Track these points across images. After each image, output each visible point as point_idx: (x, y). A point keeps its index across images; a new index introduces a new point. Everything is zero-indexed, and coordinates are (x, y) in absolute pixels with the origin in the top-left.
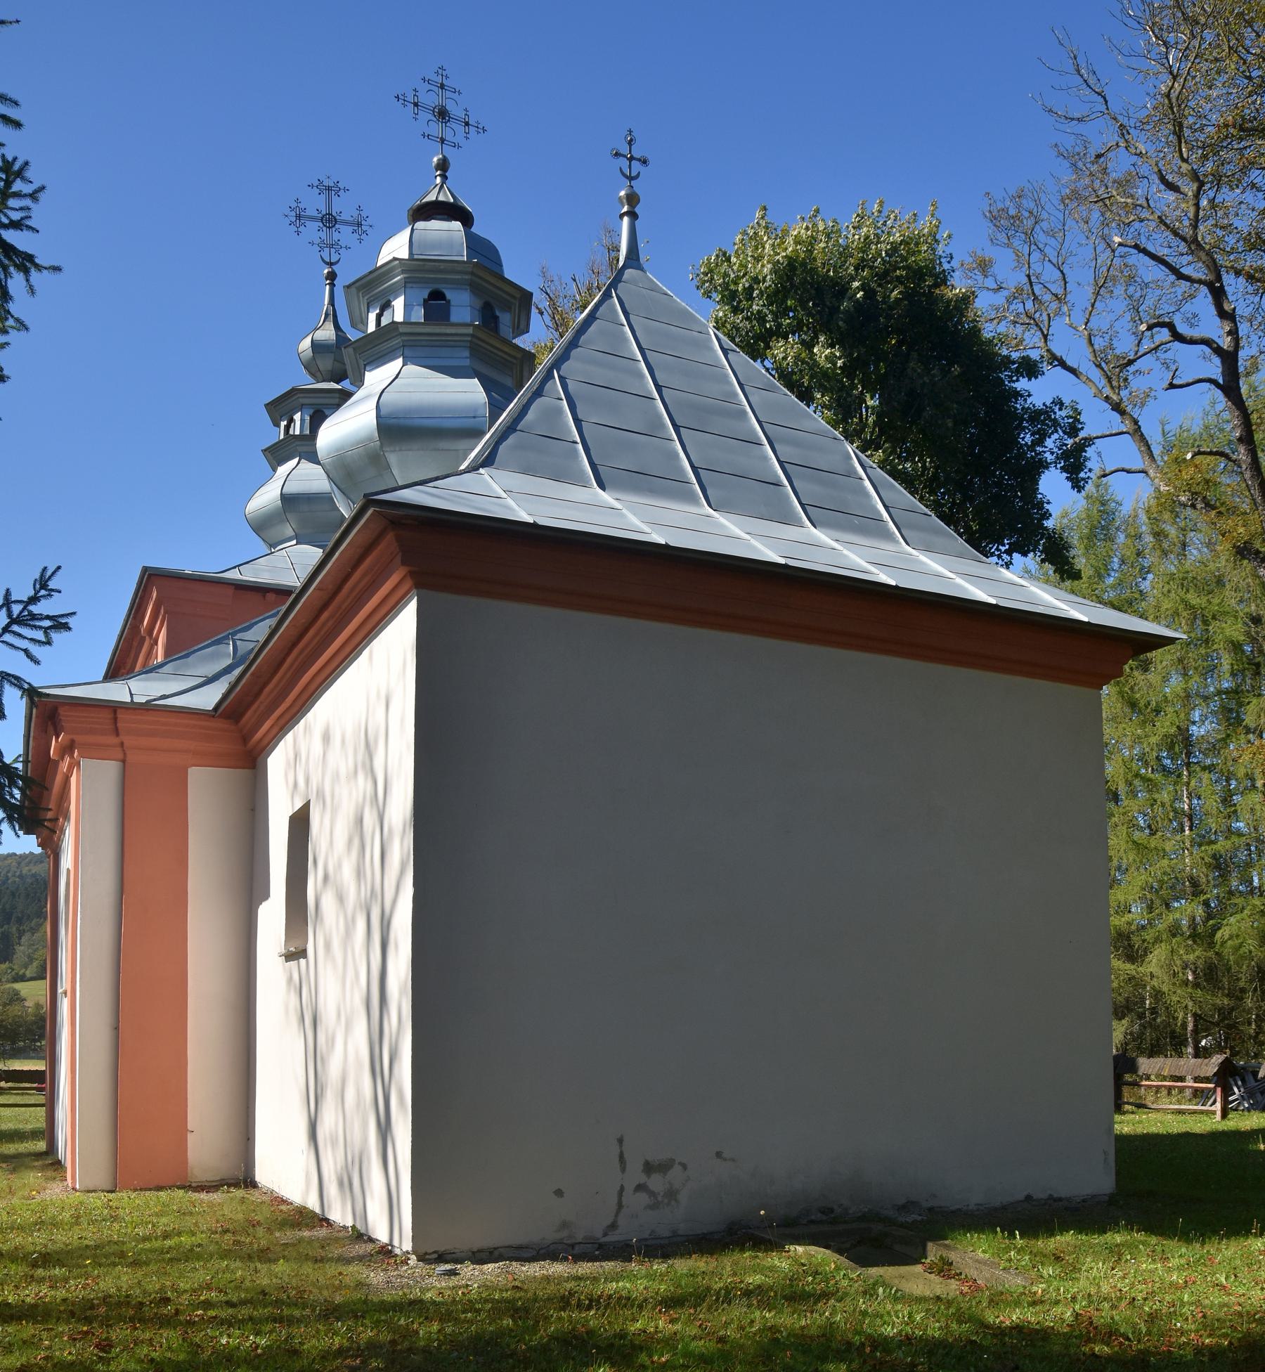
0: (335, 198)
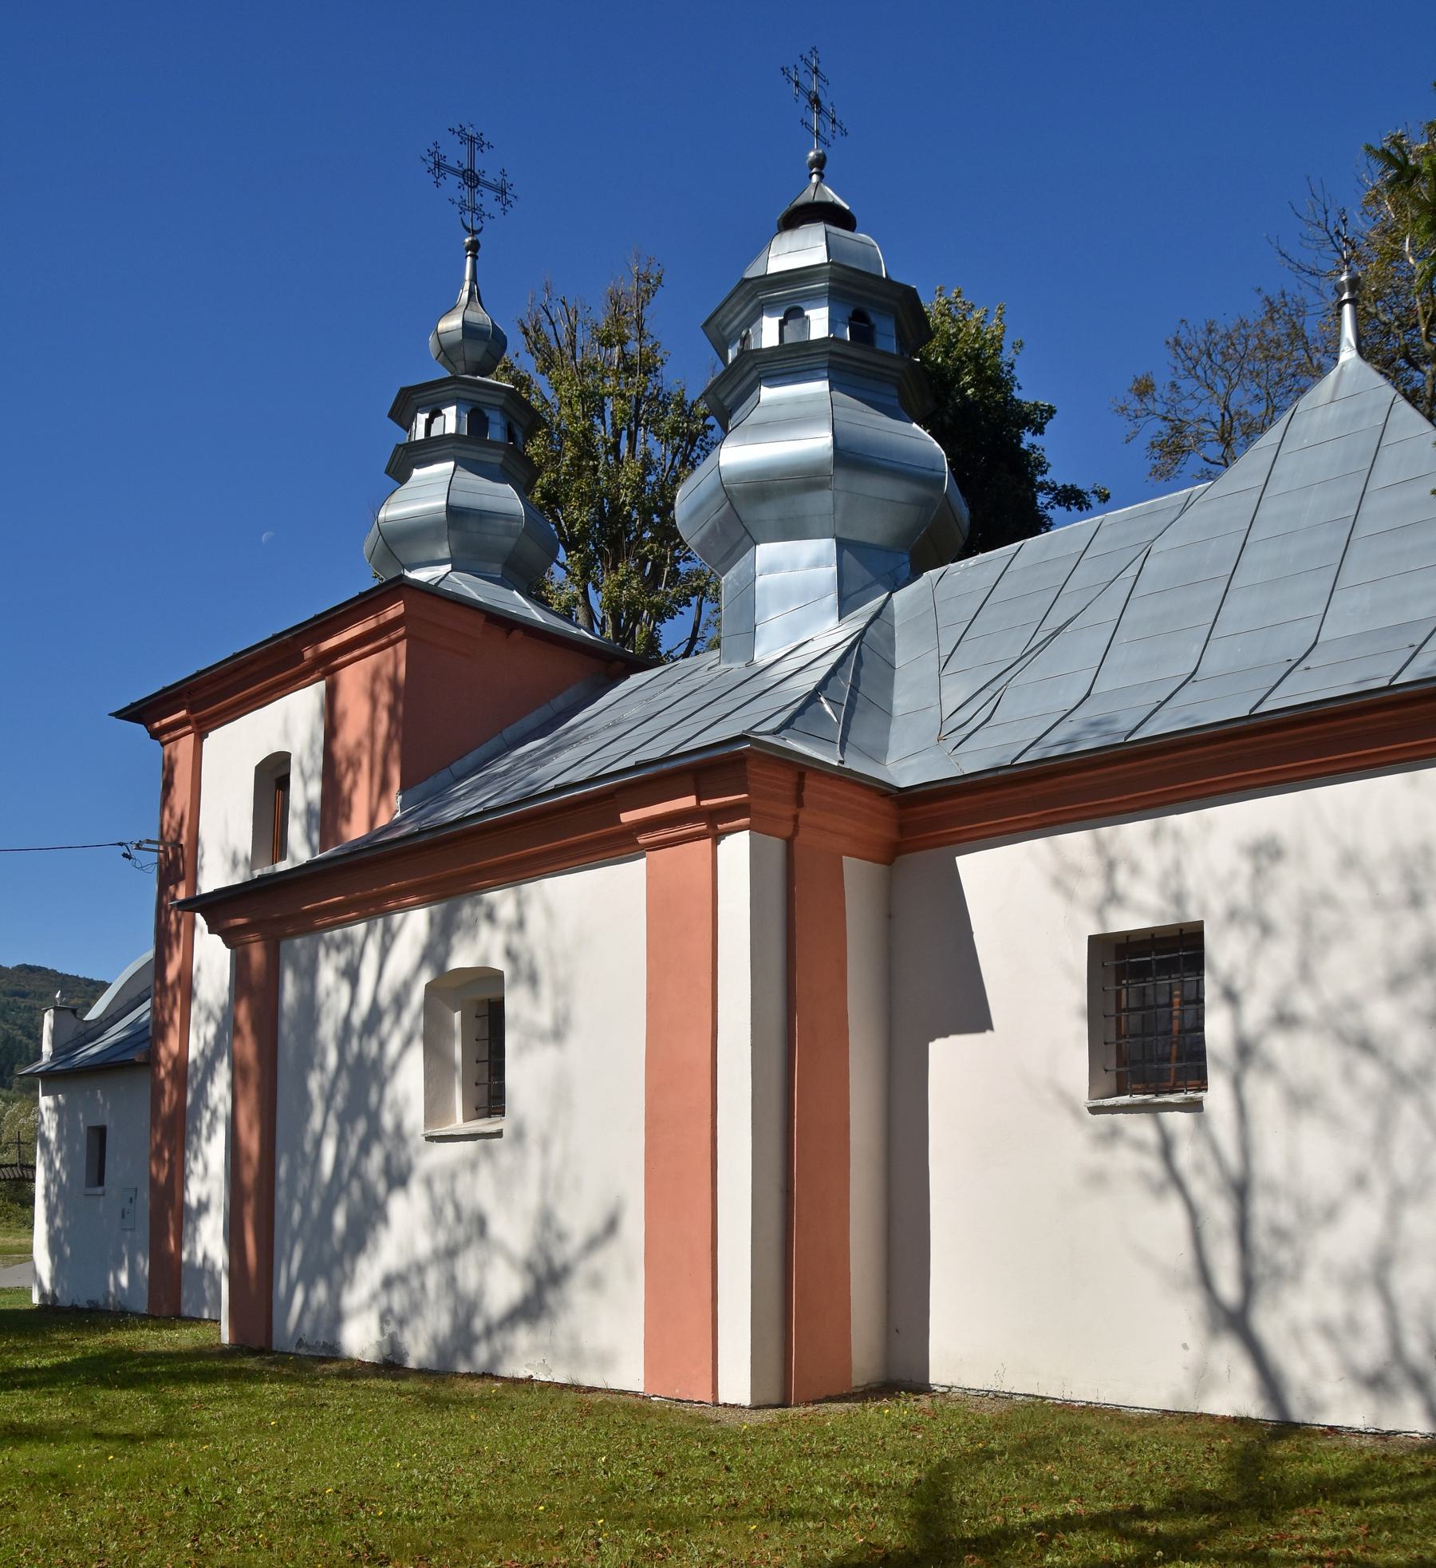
0: (478, 152)
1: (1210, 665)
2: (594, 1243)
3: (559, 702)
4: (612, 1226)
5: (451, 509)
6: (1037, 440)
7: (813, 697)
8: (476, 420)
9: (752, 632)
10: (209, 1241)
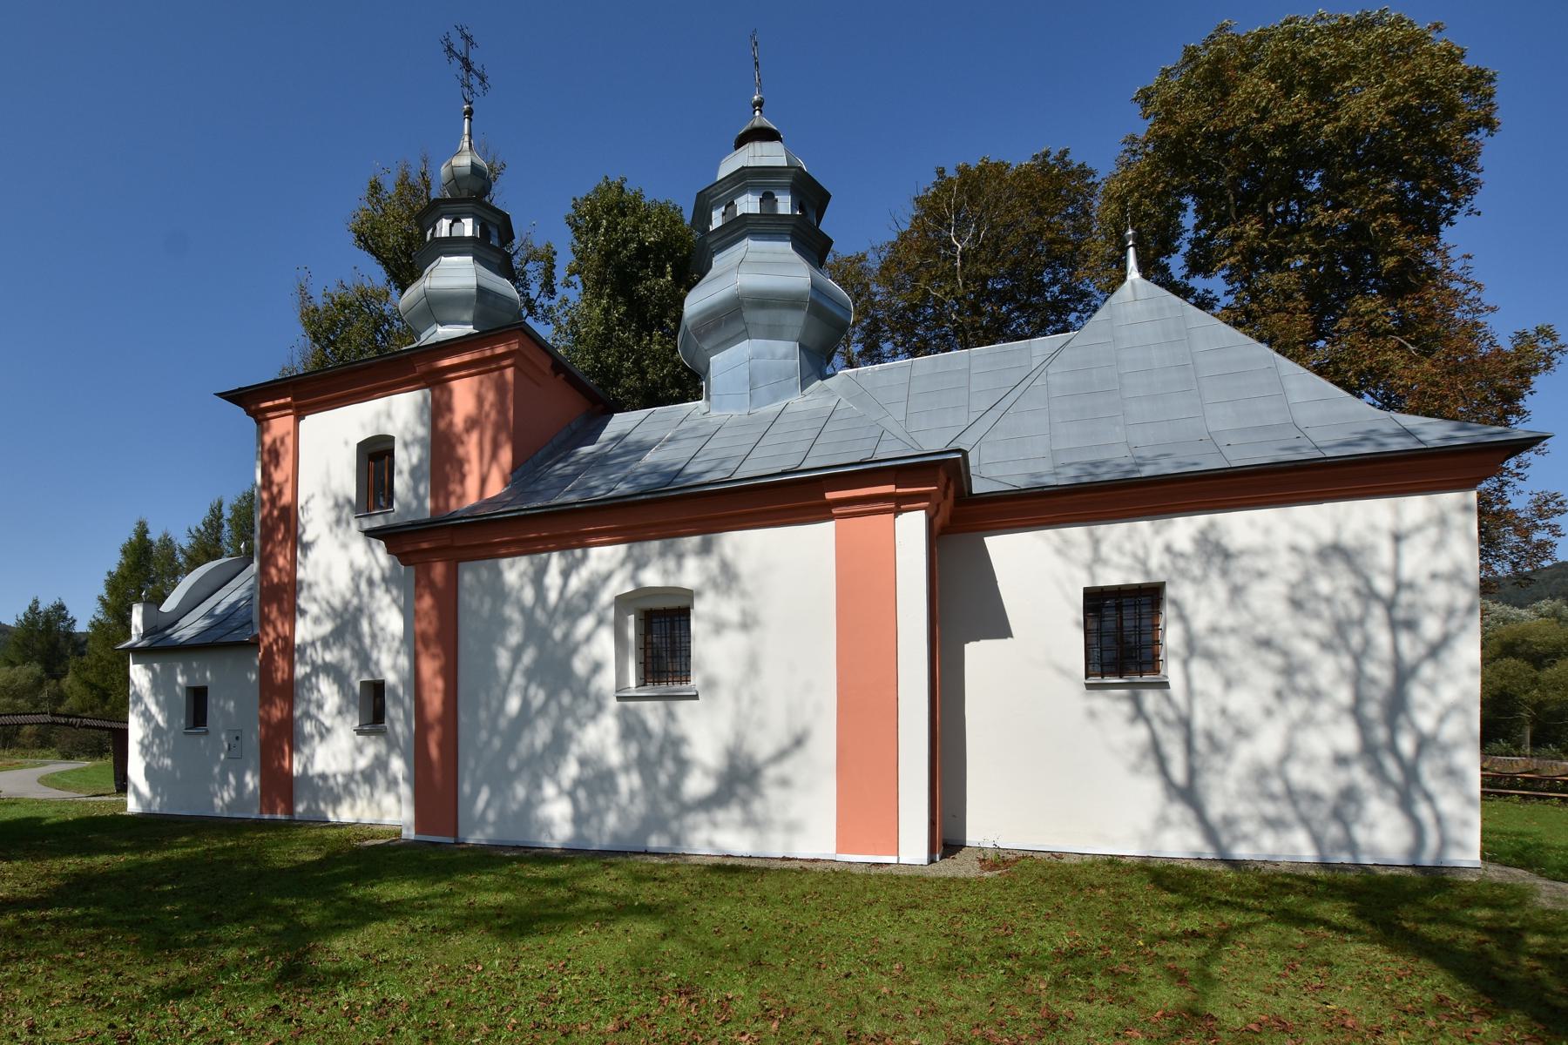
2: (781, 755)
4: (799, 742)
5: (479, 287)
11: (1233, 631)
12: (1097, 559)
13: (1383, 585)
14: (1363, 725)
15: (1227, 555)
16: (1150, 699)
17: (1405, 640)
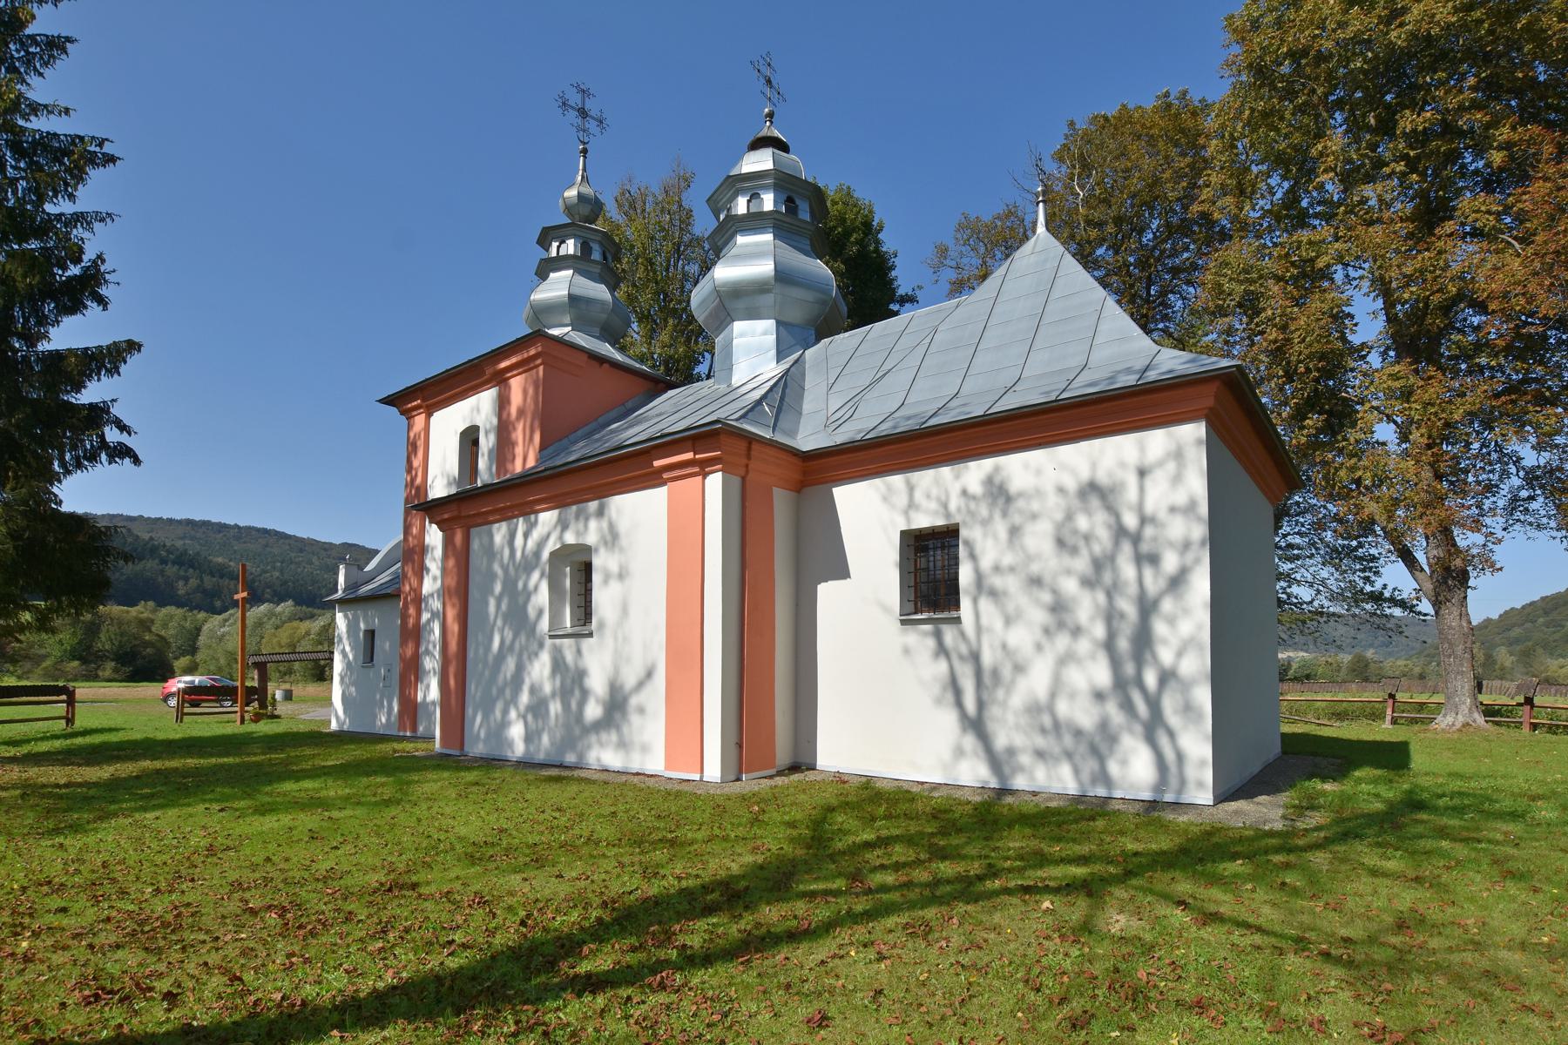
1: (966, 390)
2: (640, 685)
3: (629, 405)
4: (649, 674)
5: (570, 296)
6: (86, 235)
7: (759, 402)
8: (585, 248)
9: (731, 369)
10: (431, 691)
11: (1012, 569)
12: (912, 505)
13: (1130, 521)
14: (1115, 663)
15: (1009, 499)
16: (949, 634)
17: (1148, 573)
